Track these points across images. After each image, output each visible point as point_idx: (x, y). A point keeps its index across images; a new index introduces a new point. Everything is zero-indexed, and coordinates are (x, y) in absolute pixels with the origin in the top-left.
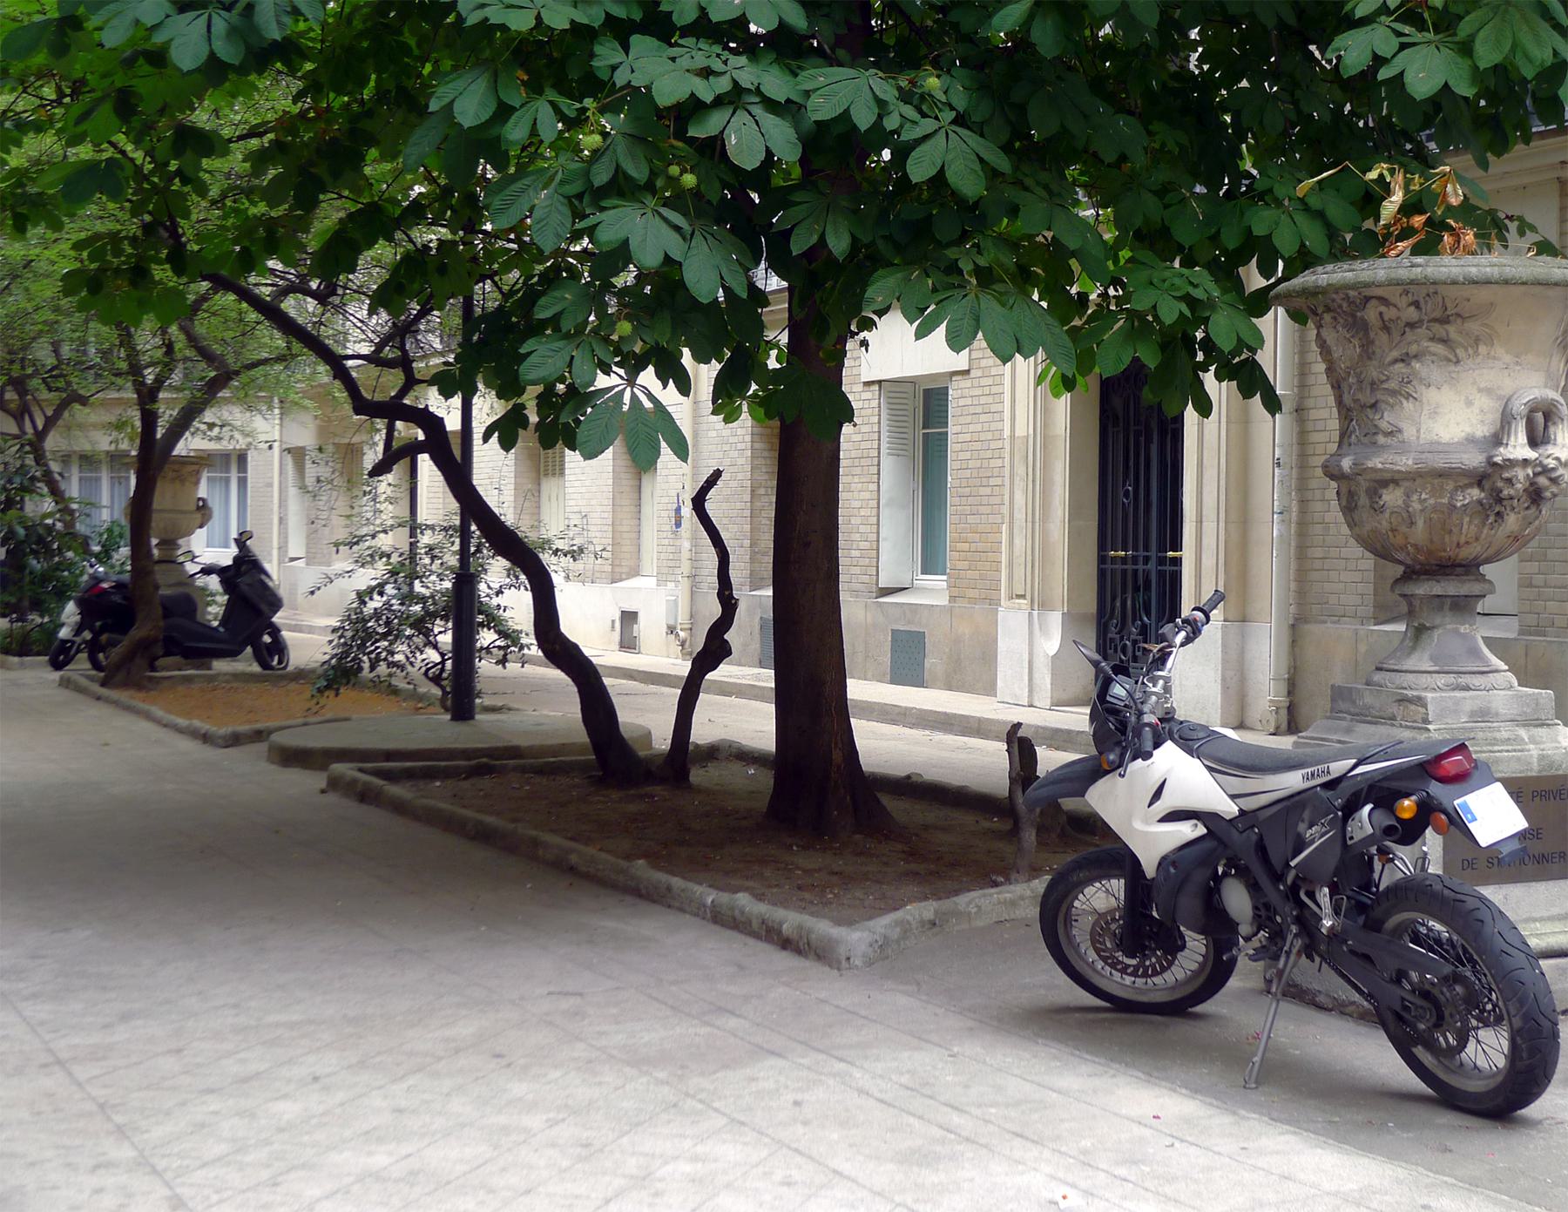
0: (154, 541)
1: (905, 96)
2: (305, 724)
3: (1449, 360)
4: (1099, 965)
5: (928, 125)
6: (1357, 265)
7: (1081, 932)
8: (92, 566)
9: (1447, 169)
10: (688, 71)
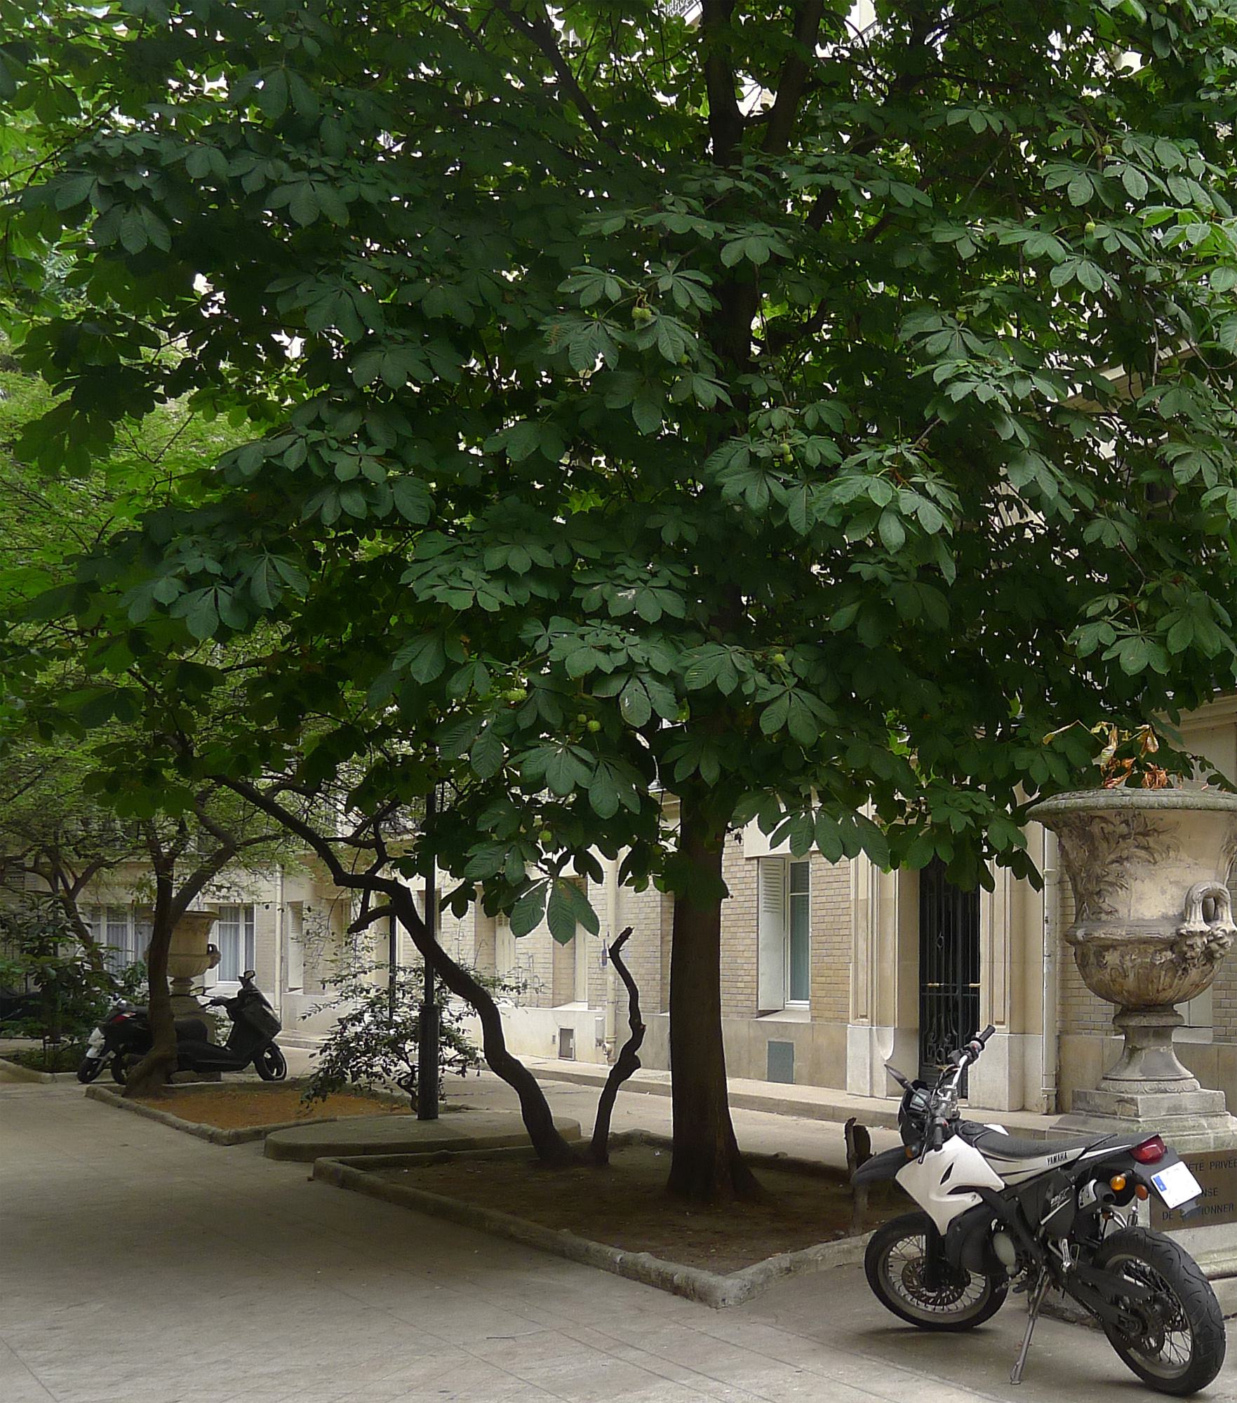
0: (170, 979)
1: (760, 666)
2: (298, 1125)
3: (1150, 862)
4: (909, 1298)
5: (776, 690)
6: (1085, 794)
7: (895, 1274)
8: (115, 999)
9: (1148, 726)
10: (595, 647)
